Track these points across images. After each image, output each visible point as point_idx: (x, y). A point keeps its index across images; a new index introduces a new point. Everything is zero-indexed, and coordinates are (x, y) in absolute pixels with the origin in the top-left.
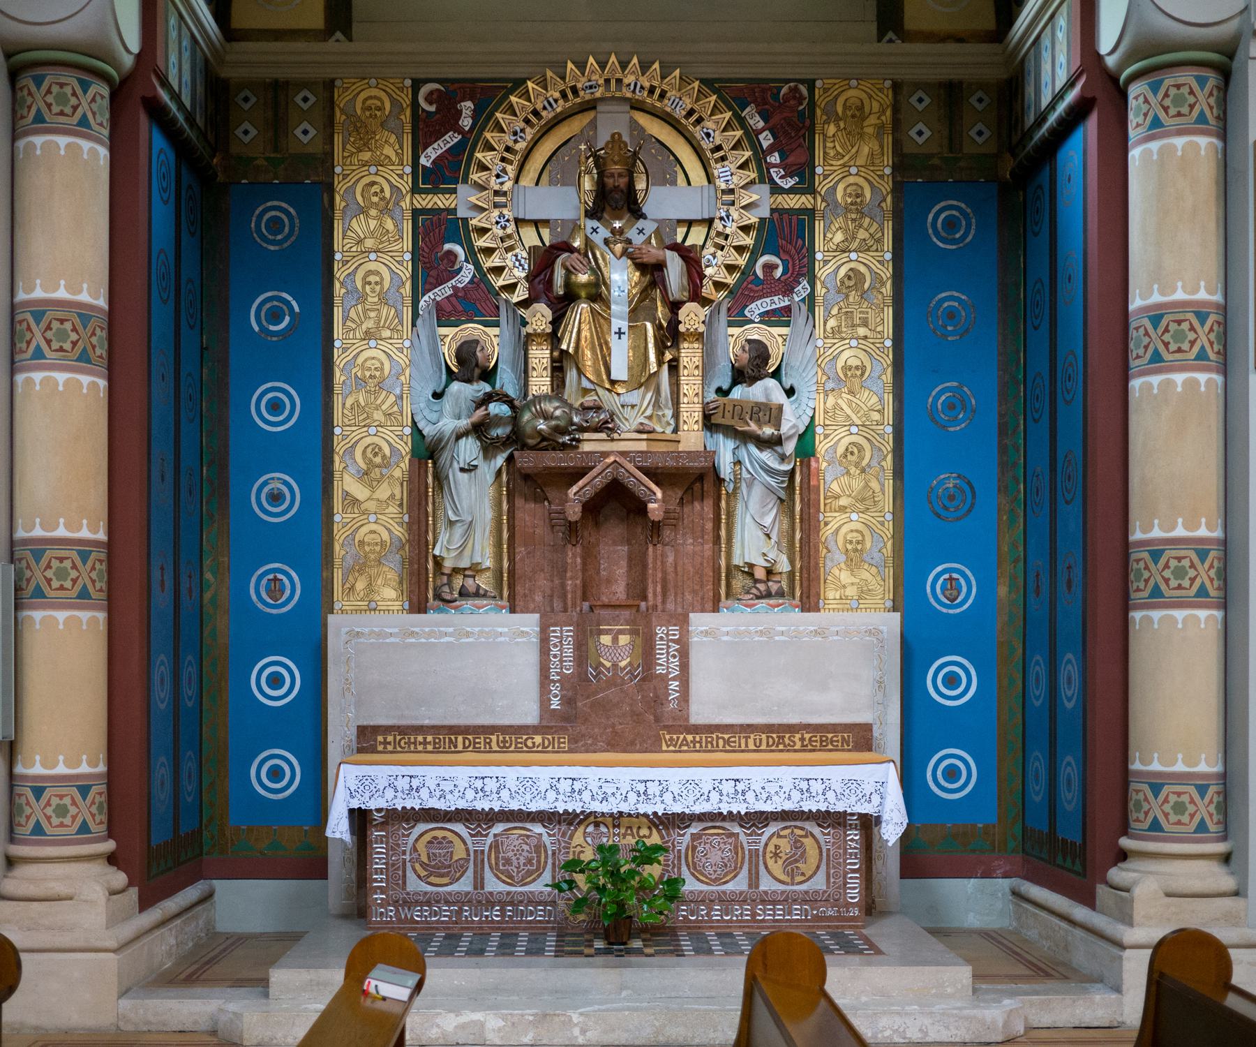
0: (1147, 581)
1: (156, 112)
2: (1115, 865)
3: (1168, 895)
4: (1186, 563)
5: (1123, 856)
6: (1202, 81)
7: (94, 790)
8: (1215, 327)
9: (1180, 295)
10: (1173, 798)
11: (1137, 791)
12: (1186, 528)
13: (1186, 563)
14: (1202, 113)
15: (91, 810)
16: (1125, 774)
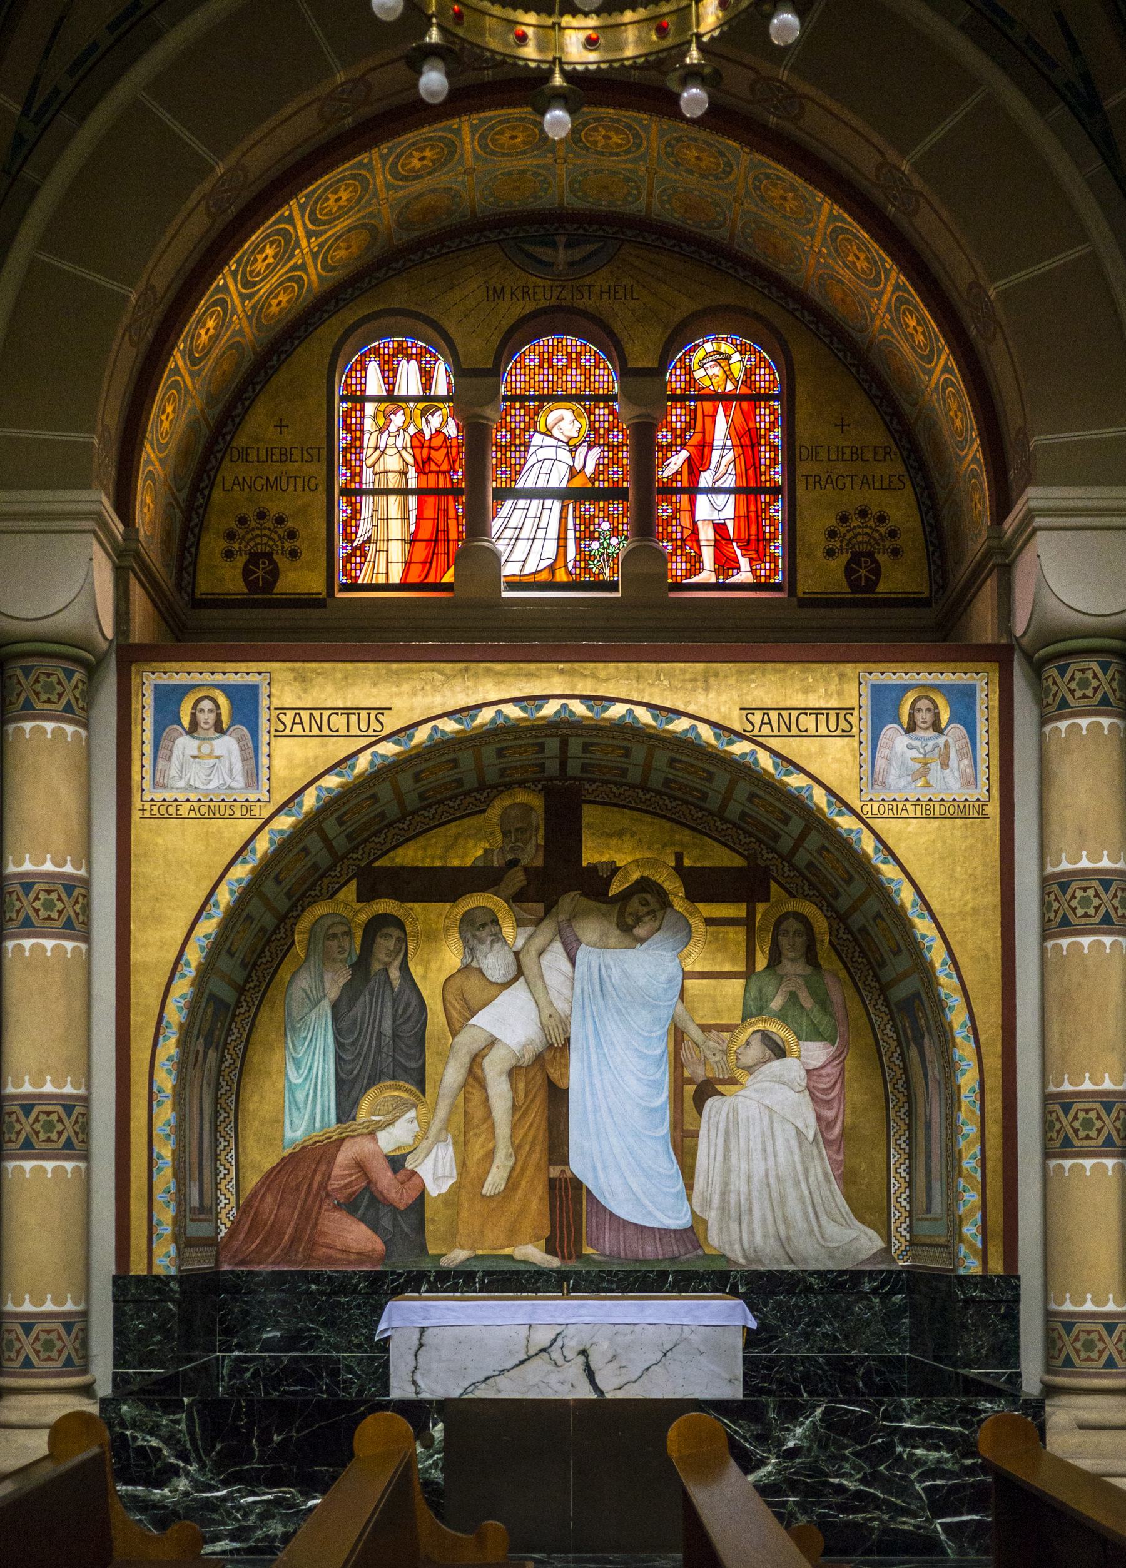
4: (1093, 1115)
6: (1105, 667)
7: (17, 1364)
10: (1083, 1336)
14: (69, 703)
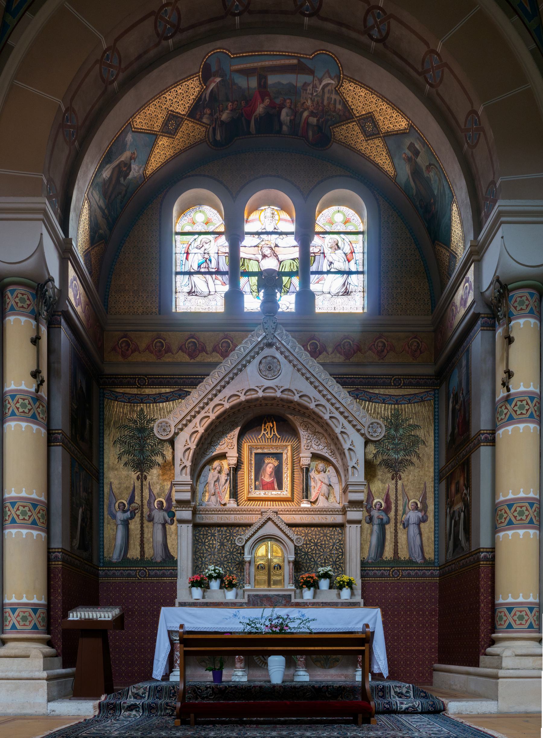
0: (505, 621)
1: (67, 316)
4: (524, 509)
5: (493, 642)
6: (531, 295)
8: (537, 404)
9: (522, 495)
11: (501, 612)
12: (524, 387)
13: (524, 509)
14: (532, 309)
16: (493, 607)
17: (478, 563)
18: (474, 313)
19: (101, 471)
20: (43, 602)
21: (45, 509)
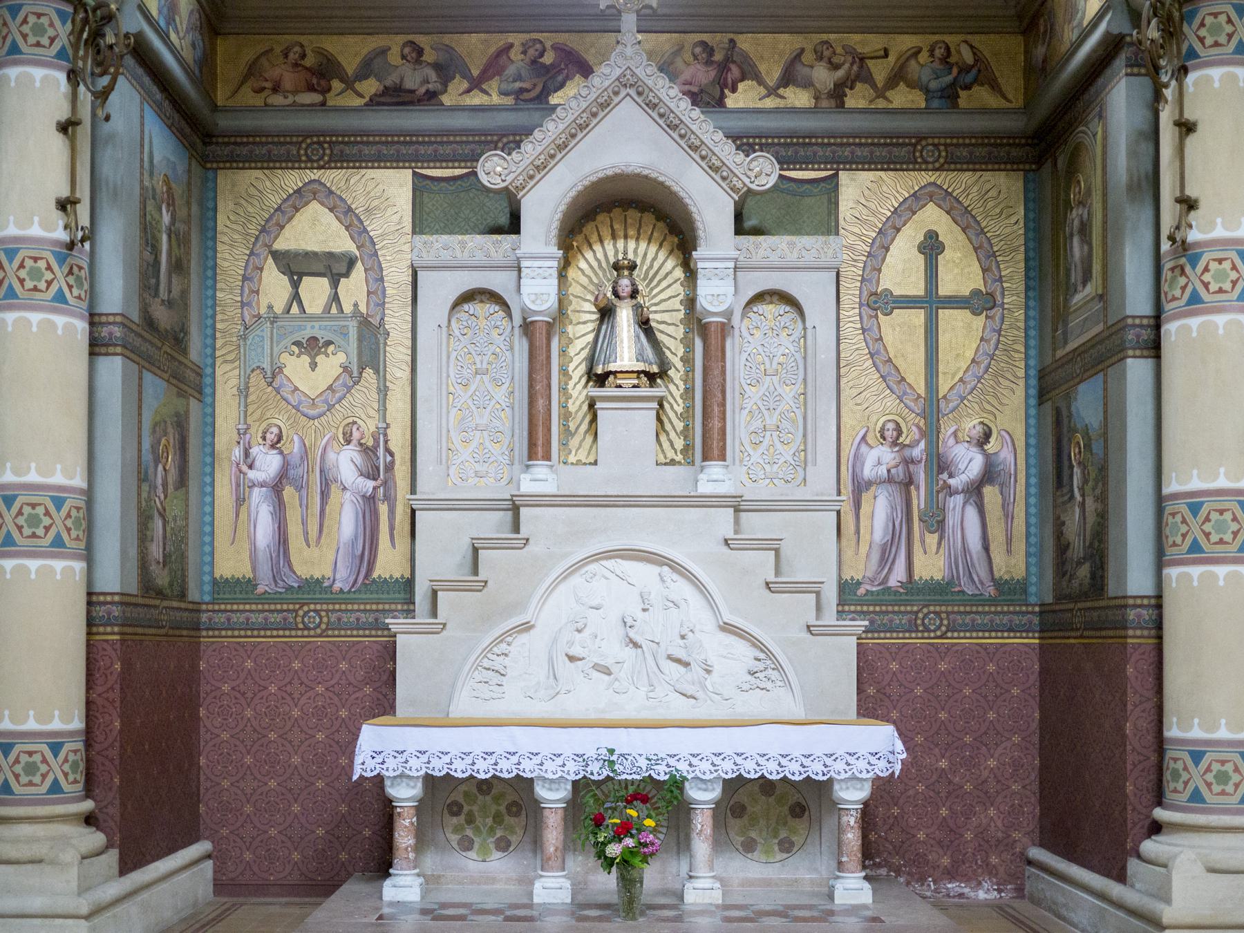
0: (66, 760)
2: (1149, 837)
3: (1212, 870)
5: (1156, 828)
11: (1175, 760)
13: (37, 758)
15: (65, 769)
16: (1160, 743)
17: (1122, 633)
18: (1107, 34)
19: (208, 370)
20: (78, 724)
21: (82, 504)
